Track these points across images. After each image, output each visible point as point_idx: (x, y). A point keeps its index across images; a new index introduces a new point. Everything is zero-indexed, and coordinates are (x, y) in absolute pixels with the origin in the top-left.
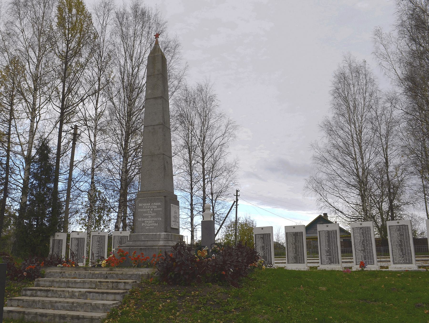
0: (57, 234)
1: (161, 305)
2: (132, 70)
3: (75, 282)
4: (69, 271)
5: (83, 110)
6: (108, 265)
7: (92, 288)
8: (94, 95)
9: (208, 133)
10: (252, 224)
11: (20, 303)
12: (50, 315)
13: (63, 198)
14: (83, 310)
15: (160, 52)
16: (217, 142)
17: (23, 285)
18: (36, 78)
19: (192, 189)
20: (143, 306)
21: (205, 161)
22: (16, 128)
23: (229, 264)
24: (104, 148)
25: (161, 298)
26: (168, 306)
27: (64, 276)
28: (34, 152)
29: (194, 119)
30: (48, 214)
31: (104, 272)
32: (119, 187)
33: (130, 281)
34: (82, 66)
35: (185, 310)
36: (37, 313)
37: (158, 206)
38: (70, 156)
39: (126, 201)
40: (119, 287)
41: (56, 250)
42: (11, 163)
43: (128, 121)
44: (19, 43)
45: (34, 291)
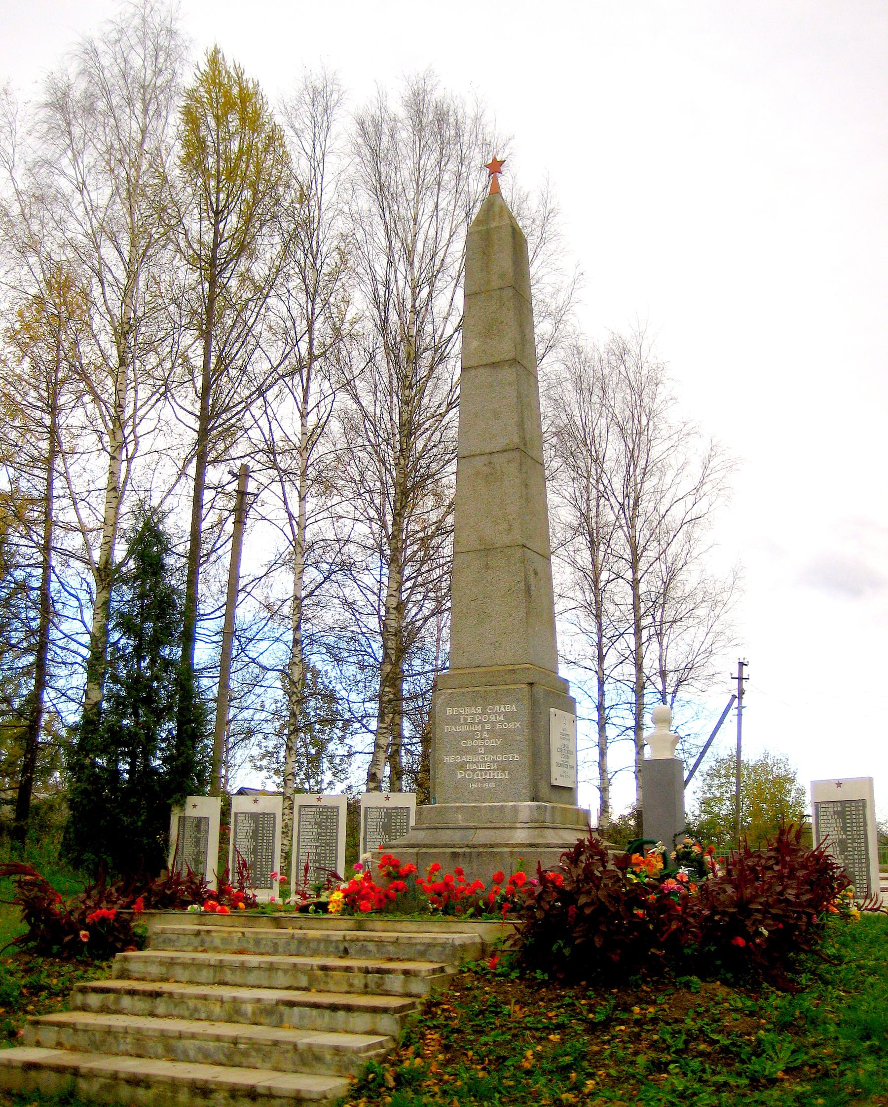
0: (191, 800)
1: (529, 1053)
2: (413, 293)
3: (244, 968)
4: (224, 927)
5: (263, 422)
6: (351, 904)
7: (298, 989)
8: (297, 377)
9: (648, 485)
10: (786, 764)
11: (66, 1036)
12: (159, 1082)
13: (208, 684)
14: (269, 1065)
15: (506, 218)
16: (677, 513)
17: (79, 973)
18: (124, 331)
19: (601, 658)
20: (470, 1053)
21: (640, 574)
22: (67, 478)
23: (757, 910)
24: (330, 535)
25: (530, 1029)
26: (555, 1059)
27: (207, 945)
28: (120, 551)
29: (604, 445)
30: (163, 740)
31: (338, 935)
32: (380, 655)
33: (423, 967)
34: (258, 289)
35: (613, 1072)
36: (116, 1072)
37: (509, 717)
38: (227, 561)
39: (398, 697)
40: (388, 987)
41: (188, 850)
42: (54, 586)
43: (401, 450)
44: (72, 225)
45: (112, 996)
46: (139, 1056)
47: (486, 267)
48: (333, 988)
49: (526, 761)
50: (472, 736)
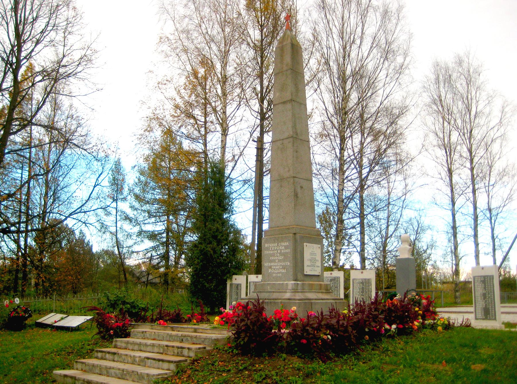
0: (235, 277)
3: (146, 345)
37: (286, 247)
45: (104, 354)
46: (100, 374)
47: (282, 62)
48: (169, 353)
49: (292, 265)
50: (273, 255)
